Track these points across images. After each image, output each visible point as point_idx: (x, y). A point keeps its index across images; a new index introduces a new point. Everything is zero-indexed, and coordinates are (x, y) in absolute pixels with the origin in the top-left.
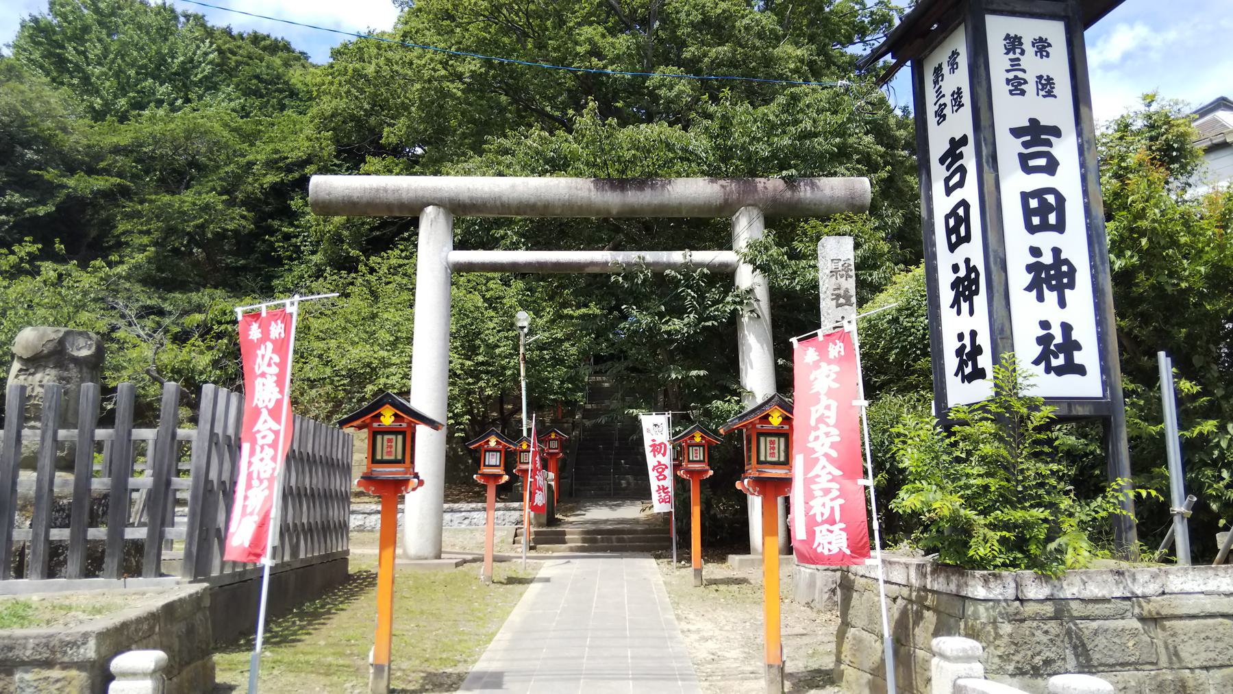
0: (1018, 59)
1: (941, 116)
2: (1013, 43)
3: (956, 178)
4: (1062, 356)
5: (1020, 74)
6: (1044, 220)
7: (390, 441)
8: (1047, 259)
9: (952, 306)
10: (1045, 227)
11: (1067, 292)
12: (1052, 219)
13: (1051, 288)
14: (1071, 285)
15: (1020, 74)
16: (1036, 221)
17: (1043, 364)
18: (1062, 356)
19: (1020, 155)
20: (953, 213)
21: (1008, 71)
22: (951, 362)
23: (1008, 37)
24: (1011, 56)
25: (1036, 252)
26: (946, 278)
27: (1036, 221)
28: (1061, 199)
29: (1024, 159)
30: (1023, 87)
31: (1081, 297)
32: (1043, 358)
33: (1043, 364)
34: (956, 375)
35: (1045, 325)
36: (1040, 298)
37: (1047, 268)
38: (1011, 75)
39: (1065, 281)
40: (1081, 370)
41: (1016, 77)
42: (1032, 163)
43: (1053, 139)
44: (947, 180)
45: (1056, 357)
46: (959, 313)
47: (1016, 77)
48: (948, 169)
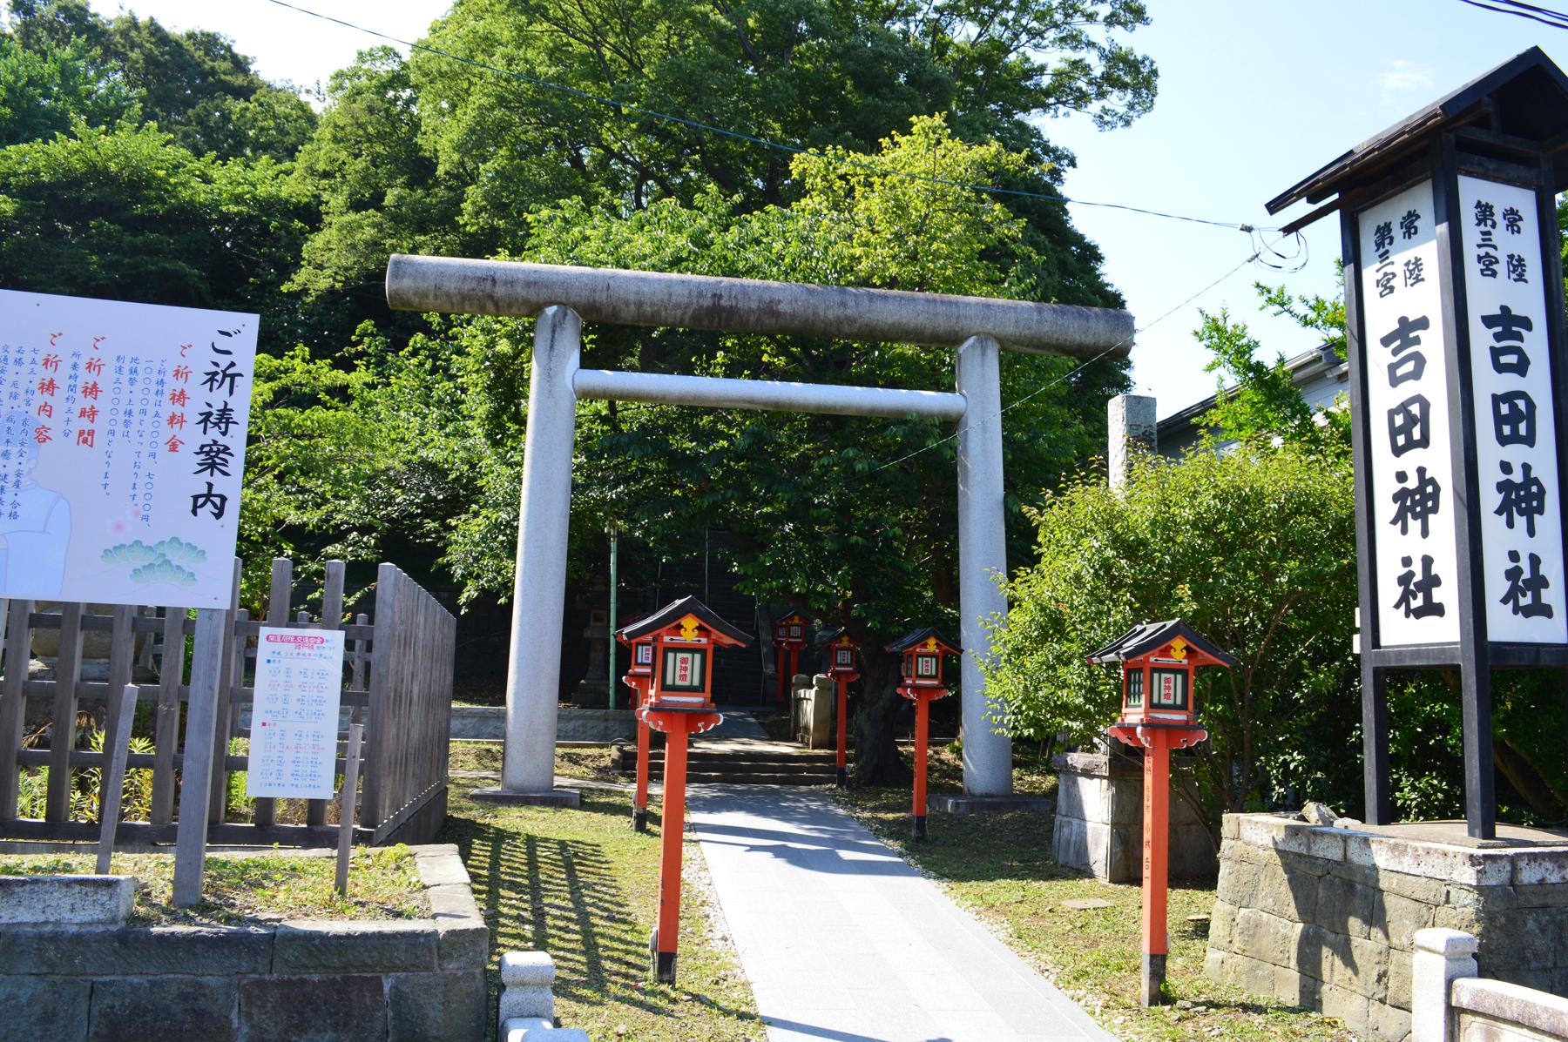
0: (1489, 233)
1: (1387, 287)
2: (1485, 212)
3: (1409, 367)
4: (1529, 594)
5: (1492, 251)
6: (1515, 430)
7: (684, 661)
8: (1517, 477)
9: (1394, 522)
10: (1514, 438)
11: (1536, 516)
12: (1416, 434)
13: (1521, 513)
14: (1540, 510)
15: (1492, 251)
16: (1507, 430)
17: (1403, 607)
18: (1529, 594)
19: (1492, 349)
20: (1403, 408)
21: (1479, 246)
22: (1389, 591)
23: (1479, 205)
24: (1482, 228)
25: (1506, 467)
26: (1385, 487)
27: (1507, 430)
28: (1531, 406)
29: (1495, 353)
30: (1494, 267)
31: (1550, 521)
32: (1405, 599)
33: (1403, 607)
34: (1397, 606)
35: (1514, 556)
36: (1510, 524)
37: (1518, 487)
38: (1482, 251)
39: (1430, 504)
40: (1547, 611)
41: (1487, 255)
42: (1504, 359)
43: (1523, 332)
44: (1392, 368)
45: (1524, 595)
46: (1404, 531)
47: (1487, 255)
48: (1395, 352)
